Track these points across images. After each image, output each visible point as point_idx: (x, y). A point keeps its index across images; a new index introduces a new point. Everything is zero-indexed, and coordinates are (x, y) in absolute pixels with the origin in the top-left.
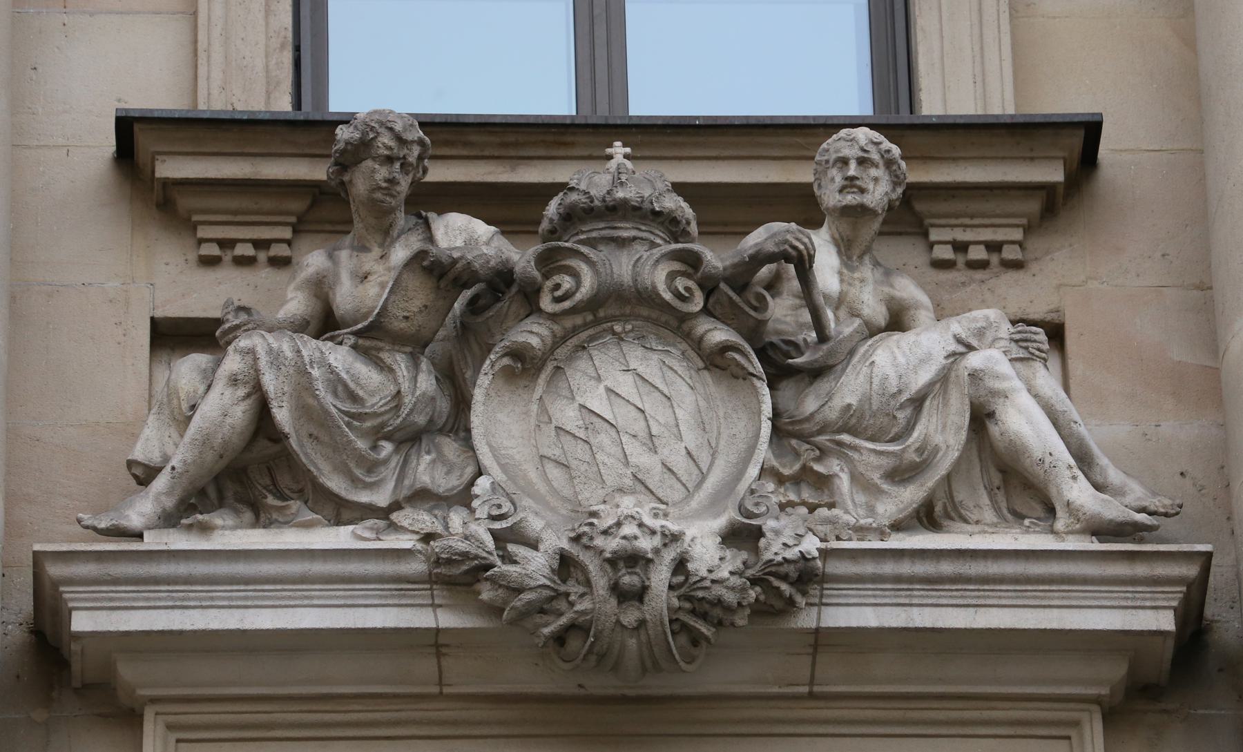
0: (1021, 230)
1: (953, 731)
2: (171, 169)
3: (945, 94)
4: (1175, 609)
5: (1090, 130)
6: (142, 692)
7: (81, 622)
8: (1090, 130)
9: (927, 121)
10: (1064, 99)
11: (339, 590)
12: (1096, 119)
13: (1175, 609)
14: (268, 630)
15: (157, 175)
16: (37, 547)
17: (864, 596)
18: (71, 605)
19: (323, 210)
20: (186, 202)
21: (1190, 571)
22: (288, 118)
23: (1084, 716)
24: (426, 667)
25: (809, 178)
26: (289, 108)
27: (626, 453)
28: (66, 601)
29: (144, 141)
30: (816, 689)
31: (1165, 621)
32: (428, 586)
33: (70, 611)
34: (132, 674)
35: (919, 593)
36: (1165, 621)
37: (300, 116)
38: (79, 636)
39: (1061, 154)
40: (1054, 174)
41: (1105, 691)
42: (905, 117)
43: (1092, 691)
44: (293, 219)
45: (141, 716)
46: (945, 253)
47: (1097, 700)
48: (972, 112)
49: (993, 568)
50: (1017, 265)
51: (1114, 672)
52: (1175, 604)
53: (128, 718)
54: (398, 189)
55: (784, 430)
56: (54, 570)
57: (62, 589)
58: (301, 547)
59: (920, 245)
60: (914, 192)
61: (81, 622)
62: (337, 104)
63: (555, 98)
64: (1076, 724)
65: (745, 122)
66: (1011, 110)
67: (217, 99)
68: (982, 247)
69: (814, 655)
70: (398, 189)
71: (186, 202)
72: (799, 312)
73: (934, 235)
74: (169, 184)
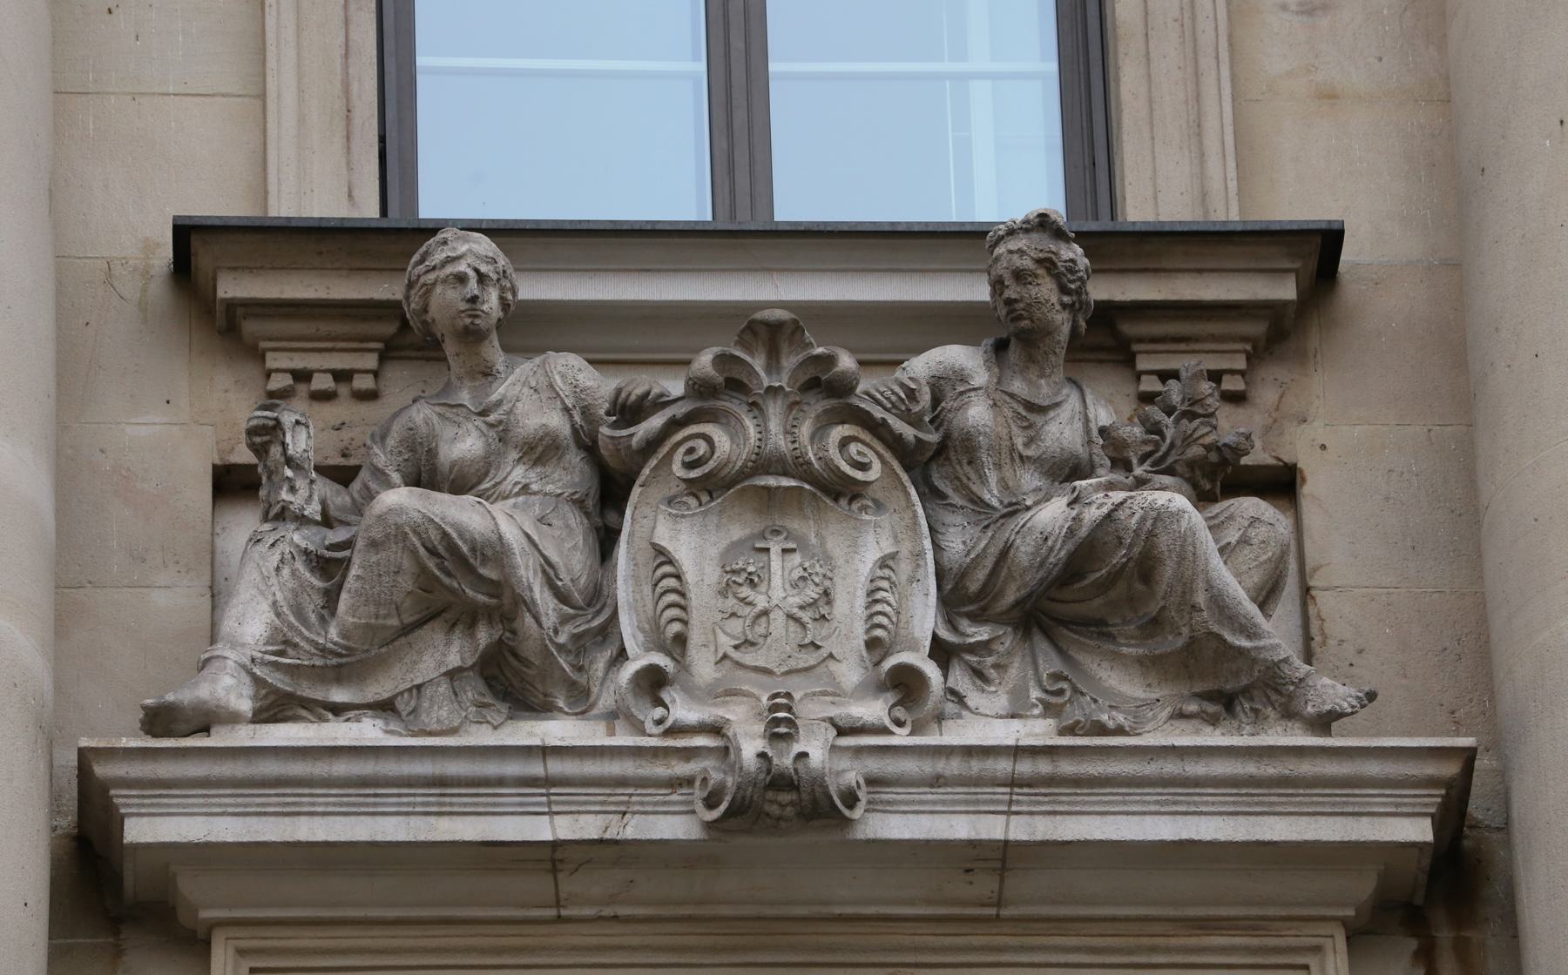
0: (1244, 357)
1: (1062, 958)
2: (231, 288)
3: (1154, 193)
4: (1432, 816)
5: (1330, 240)
6: (205, 914)
7: (140, 830)
8: (1330, 240)
9: (275, 223)
10: (1293, 204)
11: (1152, 795)
12: (1336, 227)
13: (1432, 816)
14: (1133, 841)
15: (221, 294)
16: (85, 742)
17: (288, 804)
18: (123, 811)
19: (408, 339)
20: (250, 327)
21: (1450, 769)
22: (373, 225)
23: (1328, 943)
24: (540, 885)
25: (399, 296)
26: (709, 218)
27: (794, 631)
28: (116, 807)
29: (203, 258)
30: (564, 912)
31: (1419, 831)
32: (1008, 790)
33: (122, 817)
34: (204, 899)
35: (272, 797)
36: (1419, 831)
37: (384, 224)
38: (137, 847)
39: (1297, 265)
40: (1285, 291)
41: (1350, 912)
42: (1103, 224)
43: (1340, 913)
44: (379, 345)
45: (207, 943)
46: (1150, 385)
47: (1344, 922)
48: (693, 218)
49: (319, 769)
50: (370, 396)
51: (1363, 887)
52: (1432, 810)
53: (197, 944)
54: (485, 307)
55: (816, 601)
56: (102, 770)
57: (112, 792)
58: (301, 744)
59: (251, 371)
60: (1108, 312)
61: (140, 830)
62: (429, 208)
63: (687, 200)
64: (1317, 949)
65: (924, 229)
66: (1234, 216)
67: (284, 206)
68: (330, 377)
69: (1004, 868)
70: (485, 307)
71: (250, 327)
72: (575, 458)
73: (1143, 364)
74: (232, 305)
